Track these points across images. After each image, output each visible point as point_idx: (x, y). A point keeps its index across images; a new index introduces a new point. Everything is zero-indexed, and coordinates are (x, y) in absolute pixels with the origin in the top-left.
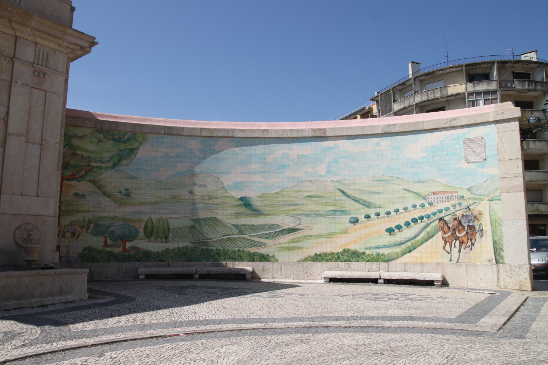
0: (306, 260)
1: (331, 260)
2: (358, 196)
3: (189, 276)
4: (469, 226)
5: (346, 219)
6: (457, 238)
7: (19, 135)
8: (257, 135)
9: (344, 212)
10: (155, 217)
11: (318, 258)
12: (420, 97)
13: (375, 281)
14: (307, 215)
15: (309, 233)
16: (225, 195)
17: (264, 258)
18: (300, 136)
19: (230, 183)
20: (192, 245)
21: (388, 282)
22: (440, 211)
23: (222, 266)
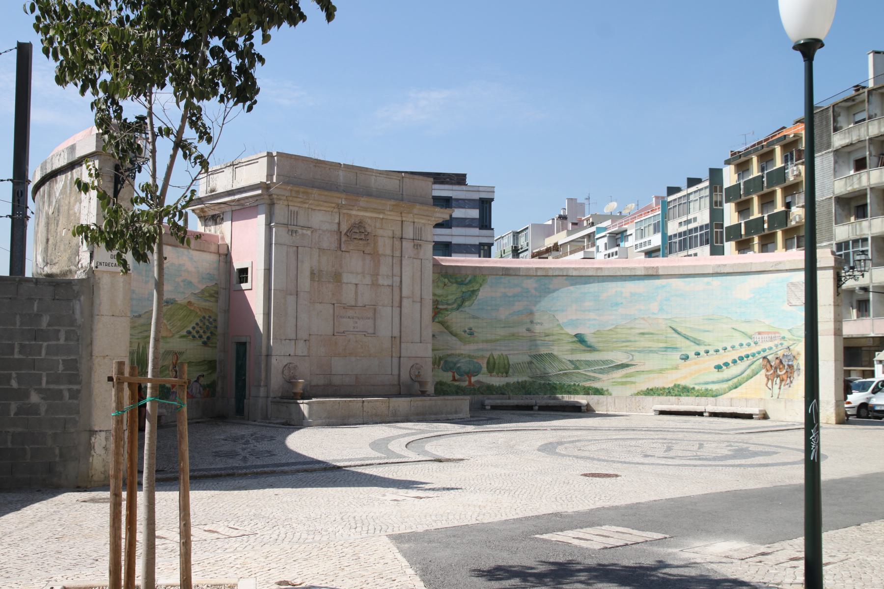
0: (638, 394)
1: (662, 394)
2: (689, 334)
3: (529, 408)
4: (788, 365)
5: (677, 356)
7: (408, 298)
8: (590, 273)
9: (675, 349)
10: (496, 354)
11: (650, 392)
12: (876, 127)
13: (701, 414)
14: (639, 352)
16: (561, 332)
17: (598, 392)
18: (633, 274)
19: (565, 321)
20: (531, 380)
22: (764, 350)
23: (557, 399)
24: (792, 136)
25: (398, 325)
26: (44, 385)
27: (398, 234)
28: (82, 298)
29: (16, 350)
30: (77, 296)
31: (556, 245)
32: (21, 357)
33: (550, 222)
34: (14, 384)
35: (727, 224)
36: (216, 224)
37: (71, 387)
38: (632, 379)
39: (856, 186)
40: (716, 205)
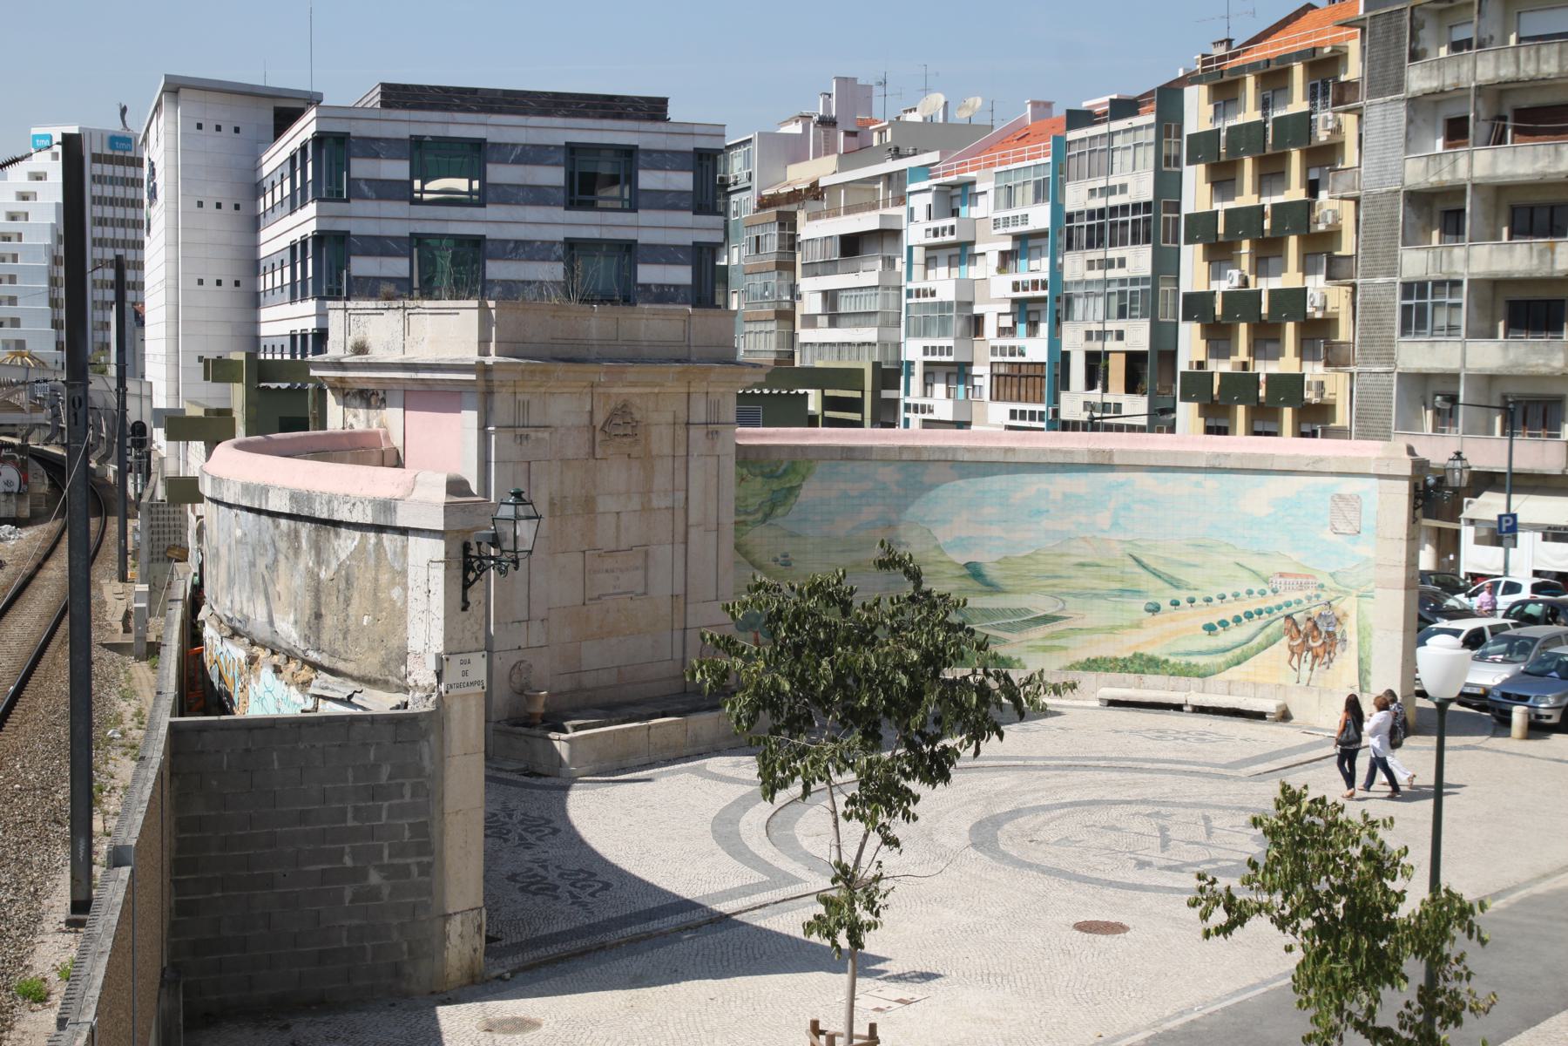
1: (1113, 669)
2: (1161, 568)
5: (1140, 605)
6: (1310, 649)
7: (698, 525)
8: (995, 458)
9: (1137, 593)
11: (1092, 665)
12: (1491, 65)
13: (1178, 708)
14: (1076, 596)
15: (1078, 624)
21: (1200, 710)
22: (1288, 605)
24: (1327, 50)
25: (682, 575)
26: (386, 860)
27: (682, 417)
28: (432, 738)
29: (350, 815)
30: (424, 735)
31: (815, 185)
32: (356, 824)
33: (796, 129)
34: (348, 861)
35: (1188, 207)
36: (369, 406)
37: (419, 859)
38: (1062, 642)
39: (1446, 178)
40: (1168, 164)
